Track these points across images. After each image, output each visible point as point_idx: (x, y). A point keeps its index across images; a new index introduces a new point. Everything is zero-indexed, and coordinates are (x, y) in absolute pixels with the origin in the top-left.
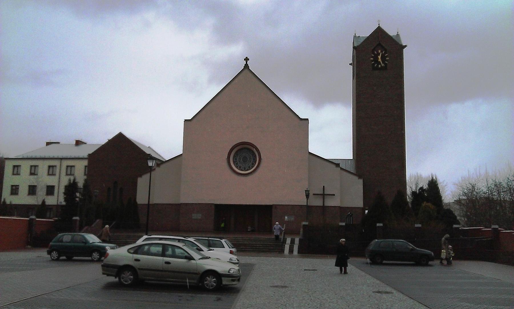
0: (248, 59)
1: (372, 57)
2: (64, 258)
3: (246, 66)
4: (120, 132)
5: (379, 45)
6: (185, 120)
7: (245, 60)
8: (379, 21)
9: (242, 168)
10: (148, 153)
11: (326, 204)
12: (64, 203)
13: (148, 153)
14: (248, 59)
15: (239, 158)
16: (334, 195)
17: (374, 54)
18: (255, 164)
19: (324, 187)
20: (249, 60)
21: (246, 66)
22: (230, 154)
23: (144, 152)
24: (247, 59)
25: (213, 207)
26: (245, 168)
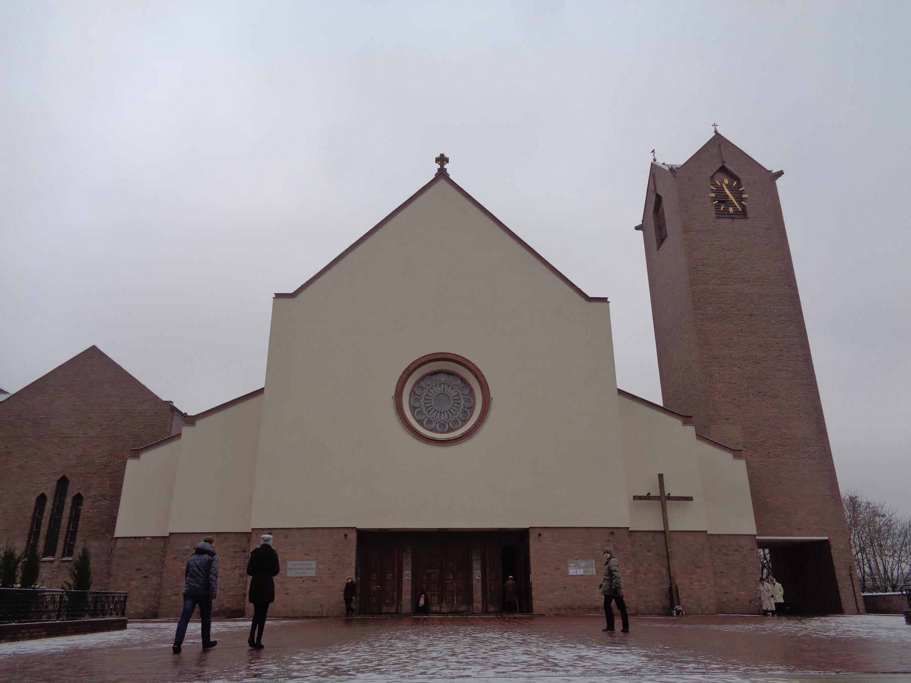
0: (447, 160)
1: (713, 191)
2: (45, 633)
3: (442, 174)
4: (93, 353)
5: (723, 169)
6: (278, 296)
7: (437, 160)
8: (715, 125)
9: (434, 425)
10: (164, 400)
11: (672, 527)
12: (782, 601)
13: (164, 399)
14: (447, 160)
15: (425, 399)
16: (690, 499)
17: (714, 184)
18: (471, 416)
19: (661, 476)
20: (448, 162)
21: (442, 174)
22: (403, 387)
23: (156, 398)
24: (442, 160)
25: (353, 536)
26: (443, 425)
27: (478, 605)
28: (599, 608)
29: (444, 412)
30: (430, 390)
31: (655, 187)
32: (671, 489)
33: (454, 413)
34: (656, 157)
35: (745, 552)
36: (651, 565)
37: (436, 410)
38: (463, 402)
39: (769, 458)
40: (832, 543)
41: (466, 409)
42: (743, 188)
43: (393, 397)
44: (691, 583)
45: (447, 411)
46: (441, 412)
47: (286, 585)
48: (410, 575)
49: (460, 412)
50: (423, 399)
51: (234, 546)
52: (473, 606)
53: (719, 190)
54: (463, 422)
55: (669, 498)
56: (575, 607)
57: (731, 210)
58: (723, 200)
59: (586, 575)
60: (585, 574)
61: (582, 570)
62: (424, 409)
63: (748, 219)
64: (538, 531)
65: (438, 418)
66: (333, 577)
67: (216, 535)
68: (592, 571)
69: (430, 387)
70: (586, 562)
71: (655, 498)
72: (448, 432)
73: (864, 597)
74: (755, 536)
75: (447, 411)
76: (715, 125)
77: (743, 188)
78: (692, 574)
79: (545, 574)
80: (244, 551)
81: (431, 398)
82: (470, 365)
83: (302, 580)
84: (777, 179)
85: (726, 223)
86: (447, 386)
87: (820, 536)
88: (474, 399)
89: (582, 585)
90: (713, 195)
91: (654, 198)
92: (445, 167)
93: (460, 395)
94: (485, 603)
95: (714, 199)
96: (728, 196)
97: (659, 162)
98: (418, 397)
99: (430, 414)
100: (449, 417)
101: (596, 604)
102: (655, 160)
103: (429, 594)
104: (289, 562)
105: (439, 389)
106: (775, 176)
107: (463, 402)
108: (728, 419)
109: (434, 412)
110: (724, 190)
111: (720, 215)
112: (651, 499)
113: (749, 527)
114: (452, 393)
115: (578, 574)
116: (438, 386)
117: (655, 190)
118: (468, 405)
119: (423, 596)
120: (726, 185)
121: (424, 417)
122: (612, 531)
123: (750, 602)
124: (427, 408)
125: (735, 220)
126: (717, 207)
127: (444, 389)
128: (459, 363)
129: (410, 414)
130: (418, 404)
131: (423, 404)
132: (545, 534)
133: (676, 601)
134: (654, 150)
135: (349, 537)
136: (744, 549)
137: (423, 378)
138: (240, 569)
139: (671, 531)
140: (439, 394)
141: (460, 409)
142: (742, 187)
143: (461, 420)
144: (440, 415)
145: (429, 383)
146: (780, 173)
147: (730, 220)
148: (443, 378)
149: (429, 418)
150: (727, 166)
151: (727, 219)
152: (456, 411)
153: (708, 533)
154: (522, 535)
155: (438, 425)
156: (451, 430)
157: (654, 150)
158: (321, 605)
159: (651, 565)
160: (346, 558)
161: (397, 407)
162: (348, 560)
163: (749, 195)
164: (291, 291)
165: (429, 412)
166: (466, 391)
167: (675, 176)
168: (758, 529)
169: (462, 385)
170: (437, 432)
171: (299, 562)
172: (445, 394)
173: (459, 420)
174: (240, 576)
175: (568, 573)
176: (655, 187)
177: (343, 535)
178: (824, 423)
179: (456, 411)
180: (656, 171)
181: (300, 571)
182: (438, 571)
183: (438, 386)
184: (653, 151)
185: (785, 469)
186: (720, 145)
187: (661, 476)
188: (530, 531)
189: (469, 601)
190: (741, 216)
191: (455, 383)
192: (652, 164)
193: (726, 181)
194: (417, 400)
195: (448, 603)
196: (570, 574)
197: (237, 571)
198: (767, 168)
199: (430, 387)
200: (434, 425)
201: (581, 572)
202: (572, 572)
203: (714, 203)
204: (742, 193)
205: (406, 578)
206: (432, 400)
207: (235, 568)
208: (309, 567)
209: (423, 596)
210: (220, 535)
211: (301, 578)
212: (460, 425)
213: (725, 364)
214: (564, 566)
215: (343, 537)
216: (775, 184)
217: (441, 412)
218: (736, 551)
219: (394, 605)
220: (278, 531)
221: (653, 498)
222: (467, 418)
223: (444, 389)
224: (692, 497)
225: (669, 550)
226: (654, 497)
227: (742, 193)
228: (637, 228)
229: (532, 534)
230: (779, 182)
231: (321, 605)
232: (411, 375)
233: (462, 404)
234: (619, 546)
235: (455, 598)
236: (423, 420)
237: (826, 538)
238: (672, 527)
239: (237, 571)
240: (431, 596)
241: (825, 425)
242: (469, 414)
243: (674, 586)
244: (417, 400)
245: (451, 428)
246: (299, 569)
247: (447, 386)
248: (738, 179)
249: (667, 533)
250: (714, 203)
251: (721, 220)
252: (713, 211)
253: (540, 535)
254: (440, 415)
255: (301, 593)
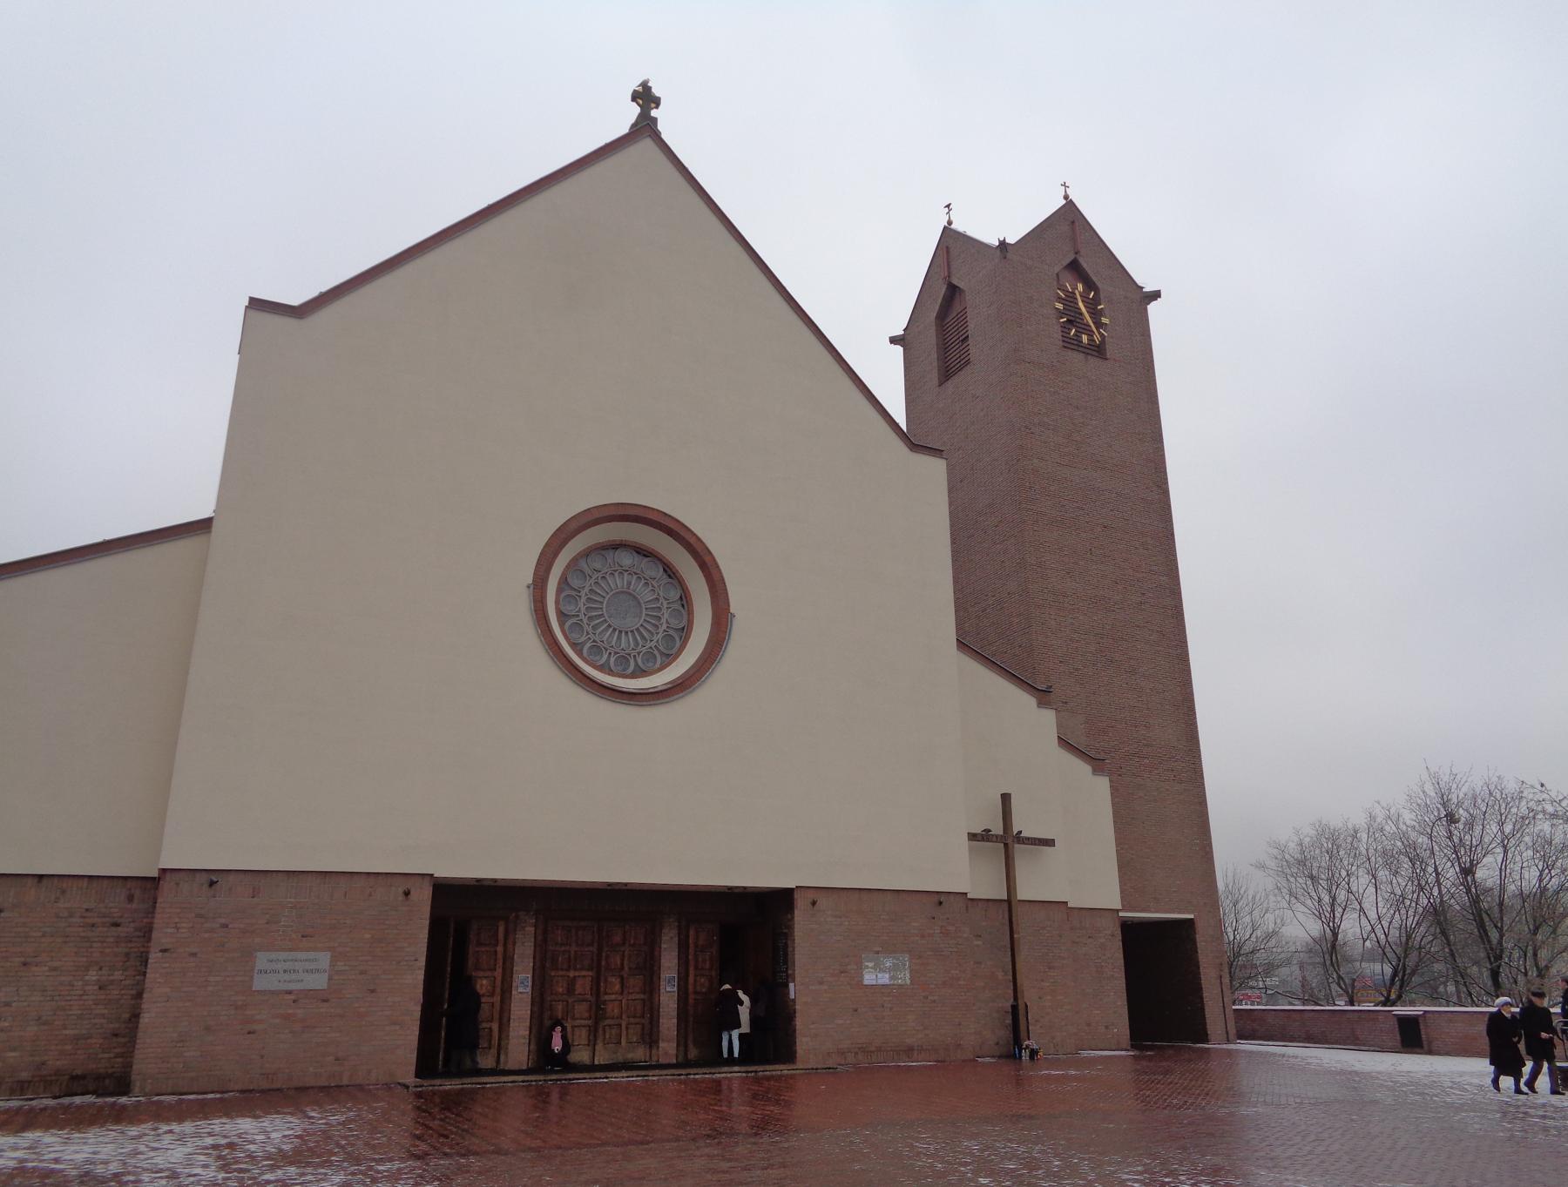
0: (657, 102)
1: (1059, 299)
3: (645, 128)
6: (256, 304)
8: (1064, 185)
11: (1023, 893)
14: (657, 102)
16: (1049, 843)
19: (1006, 798)
21: (645, 128)
24: (645, 97)
25: (423, 896)
26: (623, 660)
27: (668, 1048)
28: (913, 1050)
29: (627, 633)
30: (600, 581)
31: (949, 273)
32: (1023, 823)
33: (647, 637)
34: (952, 218)
35: (1103, 940)
36: (980, 963)
37: (610, 626)
38: (666, 616)
39: (1120, 775)
40: (1199, 926)
41: (671, 632)
42: (1102, 306)
43: (528, 587)
44: (1040, 998)
45: (632, 631)
46: (620, 632)
47: (248, 1012)
48: (530, 984)
49: (660, 636)
50: (583, 599)
51: (87, 910)
52: (658, 1047)
53: (1070, 300)
54: (664, 659)
55: (1020, 839)
56: (873, 1049)
57: (1085, 338)
58: (1074, 320)
59: (894, 985)
60: (892, 982)
61: (887, 976)
62: (585, 621)
63: (1107, 361)
64: (811, 895)
65: (613, 643)
66: (373, 991)
67: (36, 880)
68: (904, 977)
69: (600, 575)
70: (894, 958)
71: (997, 839)
72: (633, 676)
73: (1234, 1010)
74: (1118, 911)
75: (632, 631)
76: (1064, 185)
77: (1102, 306)
78: (1042, 981)
79: (821, 983)
80: (117, 925)
81: (601, 600)
82: (692, 541)
83: (292, 997)
84: (1149, 304)
85: (1076, 358)
86: (635, 577)
87: (1184, 913)
88: (690, 613)
89: (886, 1005)
90: (1060, 306)
91: (944, 290)
92: (654, 113)
93: (661, 600)
94: (682, 1041)
95: (1061, 314)
96: (1081, 314)
97: (957, 226)
98: (574, 593)
99: (598, 632)
100: (637, 644)
101: (909, 1041)
102: (950, 223)
103: (568, 1026)
104: (258, 954)
105: (619, 582)
106: (1147, 297)
107: (666, 616)
108: (1066, 703)
109: (606, 630)
110: (1078, 304)
111: (1071, 344)
112: (1024, 843)
113: (1115, 902)
114: (646, 595)
115: (880, 982)
116: (616, 574)
117: (949, 277)
118: (675, 623)
119: (559, 1029)
120: (1080, 292)
121: (583, 639)
122: (939, 899)
123: (1107, 1027)
124: (590, 618)
125: (1089, 357)
126: (1065, 328)
127: (629, 583)
128: (670, 532)
129: (559, 630)
130: (572, 607)
131: (583, 610)
132: (823, 902)
133: (1023, 1034)
134: (950, 204)
135: (414, 896)
136: (1101, 935)
137: (586, 554)
138: (101, 969)
139: (1019, 901)
140: (617, 593)
141: (661, 630)
142: (1100, 305)
143: (662, 654)
144: (619, 638)
145: (598, 565)
146: (1156, 295)
147: (1081, 356)
148: (627, 559)
149: (594, 641)
150: (1081, 261)
151: (1070, 351)
152: (652, 634)
153: (969, 896)
154: (780, 901)
155: (612, 659)
156: (640, 673)
157: (950, 204)
158: (337, 1059)
159: (980, 963)
160: (406, 945)
161: (535, 611)
162: (408, 950)
163: (1110, 321)
164: (295, 300)
165: (594, 628)
166: (674, 594)
167: (1005, 258)
168: (1123, 905)
169: (666, 579)
170: (611, 673)
171: (283, 955)
172: (630, 594)
173: (656, 652)
174: (100, 988)
175: (862, 981)
176: (949, 273)
177: (401, 890)
178: (1196, 723)
179: (652, 634)
180: (952, 245)
181: (286, 977)
182: (590, 973)
183: (616, 574)
184: (948, 206)
185: (1141, 797)
186: (1073, 222)
187: (1006, 798)
188: (796, 895)
189: (650, 1038)
190: (1094, 353)
191: (653, 574)
192: (945, 227)
193: (1080, 287)
194: (573, 599)
195: (608, 1044)
196: (866, 982)
197: (92, 976)
198: (1138, 282)
199: (600, 575)
200: (605, 656)
201: (884, 979)
202: (869, 978)
203: (1062, 320)
204: (1101, 313)
205: (521, 990)
206: (602, 603)
207: (87, 969)
208: (313, 966)
209: (559, 1029)
210: (45, 881)
211: (290, 992)
212: (658, 665)
213: (1066, 605)
214: (855, 967)
215: (401, 898)
216: (1146, 310)
217: (620, 632)
218: (1089, 937)
219: (492, 1051)
220: (231, 877)
221: (994, 839)
222: (674, 651)
223: (629, 583)
224: (1054, 840)
225: (1015, 936)
226: (997, 836)
227: (1101, 313)
228: (894, 340)
229: (799, 901)
230: (1152, 308)
231: (337, 1059)
232: (564, 547)
233: (663, 620)
234: (951, 928)
235: (624, 1033)
236: (584, 643)
237: (1191, 916)
238: (1023, 893)
239: (92, 976)
240: (573, 1027)
241: (1196, 727)
242: (678, 644)
243: (1020, 1002)
244: (573, 599)
245: (609, 664)
246: (285, 971)
247: (635, 577)
248: (1096, 290)
249: (1013, 903)
250: (1062, 320)
251: (1070, 353)
252: (1058, 335)
253: (814, 903)
254: (619, 638)
255: (287, 1031)
